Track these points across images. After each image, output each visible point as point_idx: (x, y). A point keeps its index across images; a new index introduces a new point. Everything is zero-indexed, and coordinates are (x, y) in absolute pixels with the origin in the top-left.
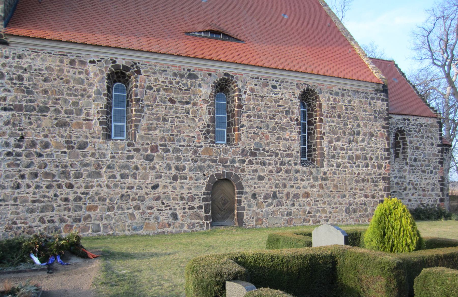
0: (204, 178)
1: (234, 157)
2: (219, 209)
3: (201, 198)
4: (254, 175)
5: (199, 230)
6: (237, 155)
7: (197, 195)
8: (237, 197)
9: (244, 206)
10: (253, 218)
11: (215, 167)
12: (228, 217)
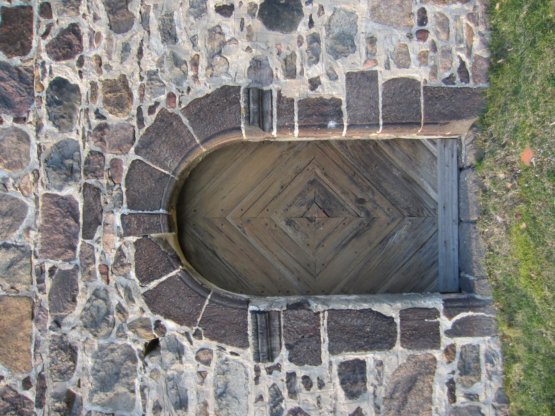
0: (168, 356)
1: (34, 154)
2: (357, 235)
3: (291, 376)
4: (145, 21)
5: (496, 384)
6: (24, 138)
7: (277, 398)
8: (284, 128)
9: (342, 81)
10: (423, 19)
11: (99, 282)
12: (409, 180)
